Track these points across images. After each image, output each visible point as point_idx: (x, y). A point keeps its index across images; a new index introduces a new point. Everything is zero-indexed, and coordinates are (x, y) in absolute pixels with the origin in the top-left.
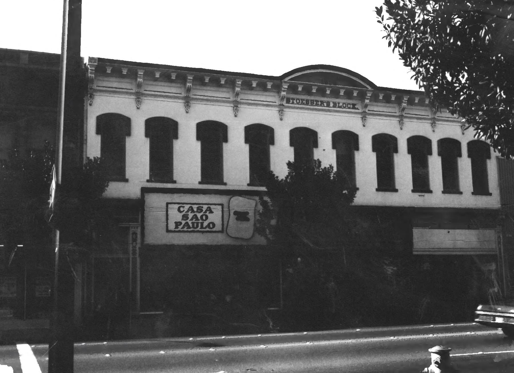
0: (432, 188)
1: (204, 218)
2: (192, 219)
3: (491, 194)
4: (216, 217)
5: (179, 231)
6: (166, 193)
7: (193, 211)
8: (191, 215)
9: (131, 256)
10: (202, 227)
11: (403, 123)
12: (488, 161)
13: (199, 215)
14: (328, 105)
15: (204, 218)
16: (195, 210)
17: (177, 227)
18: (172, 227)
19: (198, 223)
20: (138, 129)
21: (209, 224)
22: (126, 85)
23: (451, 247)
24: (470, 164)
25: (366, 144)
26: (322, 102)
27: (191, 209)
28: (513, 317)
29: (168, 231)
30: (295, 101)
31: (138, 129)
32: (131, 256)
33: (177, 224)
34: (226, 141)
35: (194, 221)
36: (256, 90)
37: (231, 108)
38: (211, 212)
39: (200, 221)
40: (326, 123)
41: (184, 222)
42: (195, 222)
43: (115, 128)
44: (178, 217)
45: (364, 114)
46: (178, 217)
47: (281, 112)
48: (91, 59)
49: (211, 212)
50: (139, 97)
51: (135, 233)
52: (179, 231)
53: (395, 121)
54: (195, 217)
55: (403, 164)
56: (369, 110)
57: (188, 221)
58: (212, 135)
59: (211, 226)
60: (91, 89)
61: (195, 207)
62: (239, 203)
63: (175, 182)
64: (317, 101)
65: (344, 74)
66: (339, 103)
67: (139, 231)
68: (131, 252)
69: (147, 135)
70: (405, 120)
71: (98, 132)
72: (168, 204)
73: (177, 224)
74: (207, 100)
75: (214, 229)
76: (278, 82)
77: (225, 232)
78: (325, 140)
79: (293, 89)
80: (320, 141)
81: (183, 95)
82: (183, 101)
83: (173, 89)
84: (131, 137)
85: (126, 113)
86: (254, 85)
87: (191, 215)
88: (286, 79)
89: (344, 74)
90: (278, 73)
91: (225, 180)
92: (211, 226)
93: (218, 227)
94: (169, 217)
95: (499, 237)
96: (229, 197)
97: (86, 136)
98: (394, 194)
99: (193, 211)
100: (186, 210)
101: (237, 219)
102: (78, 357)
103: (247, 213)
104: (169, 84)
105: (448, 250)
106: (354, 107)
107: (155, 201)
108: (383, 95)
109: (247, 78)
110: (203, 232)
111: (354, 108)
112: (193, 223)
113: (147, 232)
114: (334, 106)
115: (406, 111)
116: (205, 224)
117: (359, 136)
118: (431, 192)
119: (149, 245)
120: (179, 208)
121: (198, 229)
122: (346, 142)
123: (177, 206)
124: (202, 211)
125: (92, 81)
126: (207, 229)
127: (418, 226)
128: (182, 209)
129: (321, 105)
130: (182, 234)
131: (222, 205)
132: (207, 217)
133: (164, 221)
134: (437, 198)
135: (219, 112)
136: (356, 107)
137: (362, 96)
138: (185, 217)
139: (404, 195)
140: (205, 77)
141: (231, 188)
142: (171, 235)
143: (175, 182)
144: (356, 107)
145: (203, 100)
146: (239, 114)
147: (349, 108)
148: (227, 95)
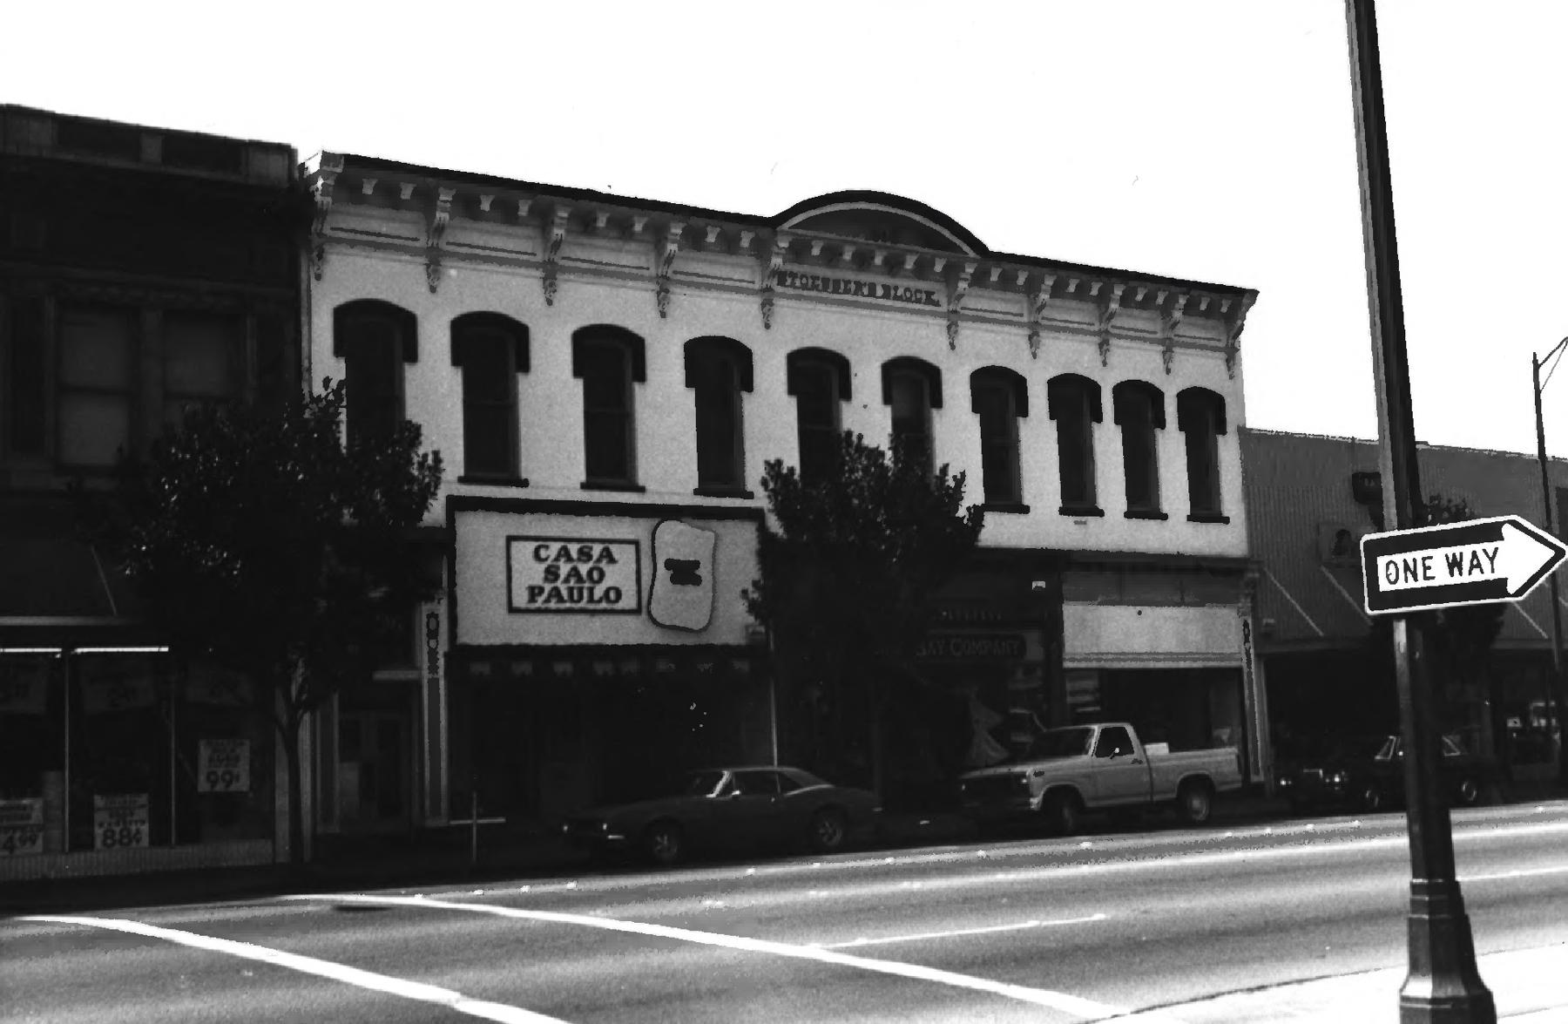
0: (1101, 503)
1: (596, 575)
2: (567, 580)
3: (1226, 521)
4: (620, 575)
5: (539, 611)
6: (608, 514)
7: (569, 559)
8: (564, 569)
9: (426, 674)
10: (591, 600)
11: (1171, 358)
12: (1220, 438)
13: (584, 569)
14: (872, 294)
15: (596, 575)
16: (574, 555)
17: (532, 599)
18: (521, 599)
19: (581, 590)
20: (435, 340)
21: (608, 591)
22: (629, 257)
23: (1148, 650)
24: (1183, 448)
25: (771, 374)
26: (859, 285)
27: (564, 553)
30: (798, 283)
31: (435, 340)
32: (426, 674)
33: (534, 592)
35: (572, 583)
36: (604, 237)
37: (422, 269)
38: (612, 560)
39: (587, 585)
40: (869, 337)
41: (548, 587)
42: (573, 590)
45: (953, 317)
47: (767, 305)
48: (327, 158)
49: (612, 560)
51: (433, 616)
52: (539, 611)
53: (1019, 336)
54: (575, 572)
55: (1039, 442)
56: (675, 272)
57: (559, 584)
58: (609, 360)
59: (612, 595)
60: (320, 235)
61: (574, 549)
62: (677, 540)
63: (524, 483)
64: (847, 282)
65: (917, 218)
66: (896, 288)
67: (442, 609)
68: (426, 665)
69: (791, 392)
70: (1177, 350)
72: (510, 539)
73: (534, 592)
74: (596, 273)
75: (620, 605)
76: (765, 232)
77: (644, 610)
78: (867, 382)
79: (798, 251)
80: (855, 382)
81: (422, 243)
82: (423, 260)
83: (518, 241)
84: (419, 364)
85: (632, 325)
87: (564, 569)
88: (786, 226)
89: (917, 218)
90: (769, 211)
92: (612, 595)
93: (629, 601)
94: (515, 575)
95: (1246, 625)
96: (657, 521)
98: (1022, 518)
99: (569, 559)
100: (553, 556)
101: (674, 580)
102: (1457, 836)
103: (696, 564)
104: (393, 213)
105: (1137, 656)
106: (929, 300)
107: (480, 537)
108: (751, 235)
110: (594, 612)
111: (929, 301)
112: (571, 590)
114: (886, 296)
116: (599, 592)
117: (648, 342)
118: (1100, 513)
120: (537, 551)
121: (582, 604)
122: (912, 384)
124: (590, 557)
125: (322, 214)
126: (604, 605)
127: (1078, 598)
128: (543, 553)
129: (856, 293)
131: (636, 543)
132: (602, 575)
133: (500, 586)
134: (1113, 529)
135: (507, 291)
136: (934, 297)
137: (951, 275)
138: (552, 574)
139: (1041, 522)
140: (403, 185)
143: (524, 483)
144: (934, 297)
146: (556, 298)
147: (918, 301)
148: (642, 262)
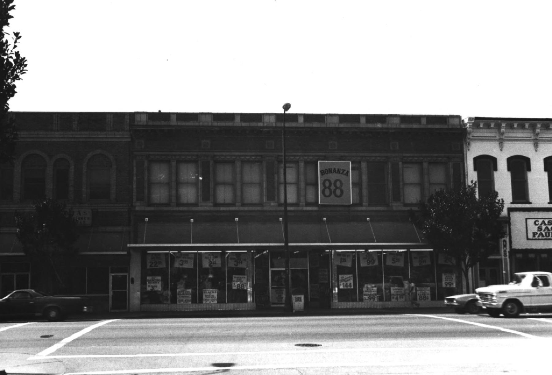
2: (544, 230)
7: (545, 224)
8: (544, 227)
17: (534, 236)
19: (549, 233)
20: (502, 165)
28: (550, 323)
29: (528, 239)
31: (502, 165)
33: (534, 234)
34: (529, 170)
41: (539, 233)
43: (486, 165)
44: (535, 229)
46: (535, 229)
48: (470, 119)
50: (501, 142)
51: (505, 241)
54: (547, 228)
57: (542, 232)
60: (469, 139)
61: (546, 221)
67: (507, 240)
68: (503, 254)
71: (475, 169)
72: (526, 219)
73: (534, 234)
86: (515, 126)
87: (544, 227)
91: (531, 200)
97: (467, 172)
99: (545, 224)
107: (518, 219)
109: (545, 122)
112: (546, 233)
113: (513, 240)
115: (540, 136)
119: (515, 249)
123: (534, 220)
128: (537, 223)
130: (538, 241)
135: (523, 149)
138: (540, 229)
141: (535, 207)
142: (530, 241)
143: (531, 203)
145: (488, 139)
146: (538, 149)
